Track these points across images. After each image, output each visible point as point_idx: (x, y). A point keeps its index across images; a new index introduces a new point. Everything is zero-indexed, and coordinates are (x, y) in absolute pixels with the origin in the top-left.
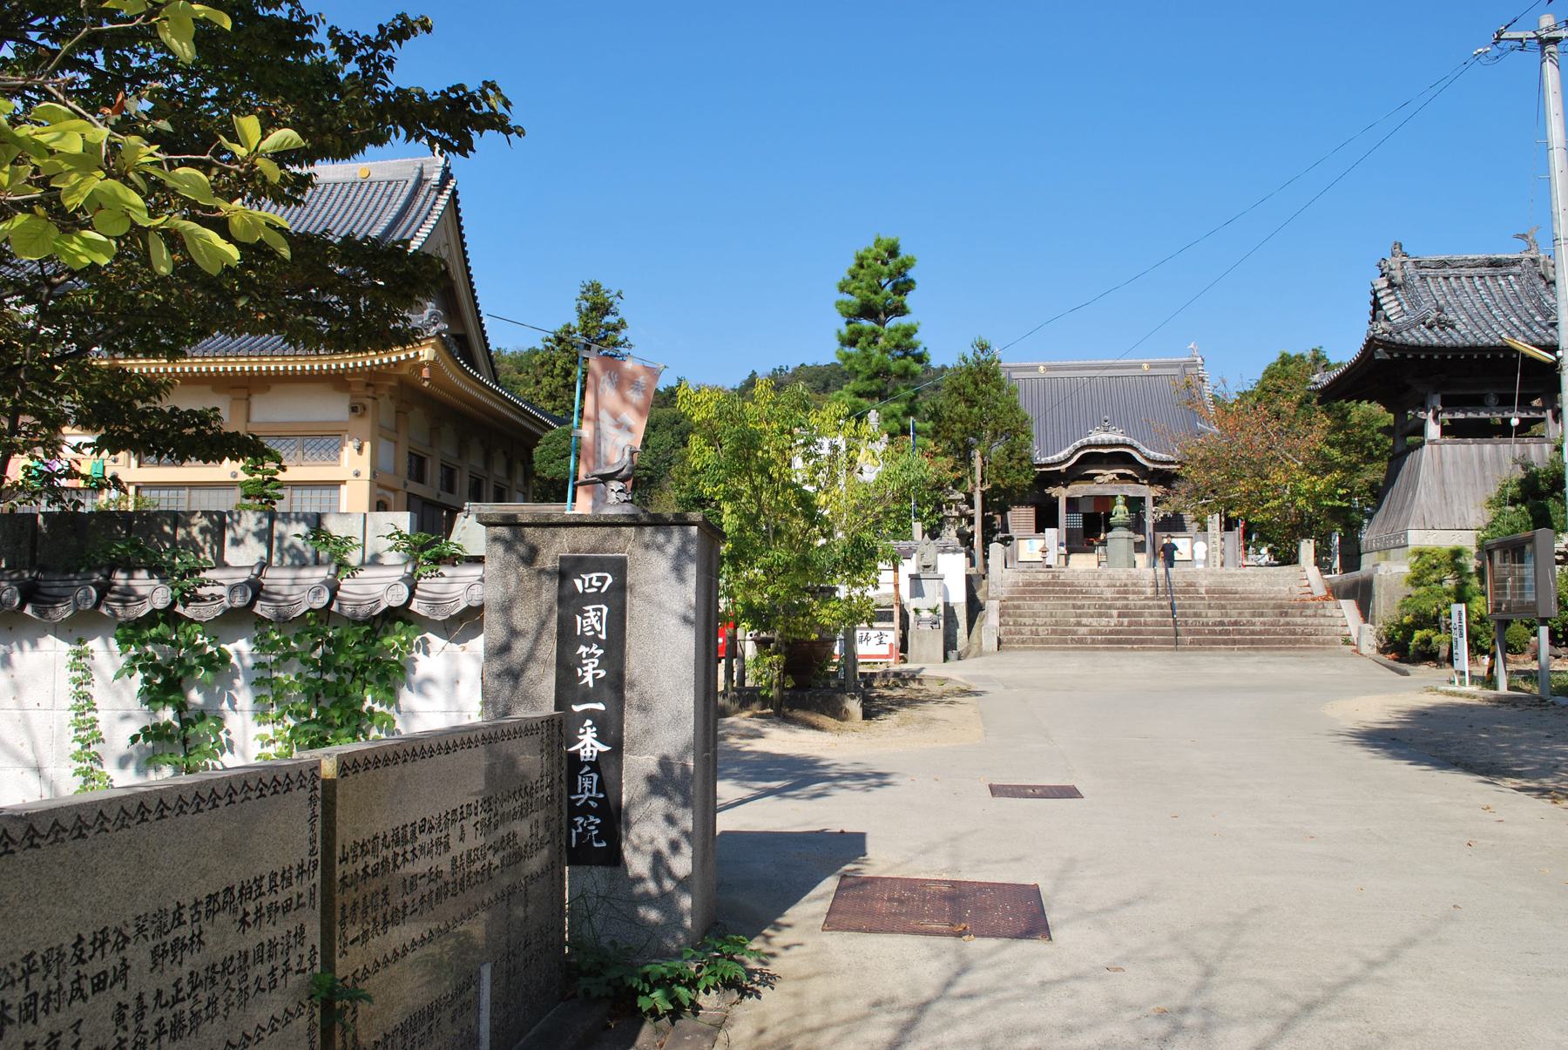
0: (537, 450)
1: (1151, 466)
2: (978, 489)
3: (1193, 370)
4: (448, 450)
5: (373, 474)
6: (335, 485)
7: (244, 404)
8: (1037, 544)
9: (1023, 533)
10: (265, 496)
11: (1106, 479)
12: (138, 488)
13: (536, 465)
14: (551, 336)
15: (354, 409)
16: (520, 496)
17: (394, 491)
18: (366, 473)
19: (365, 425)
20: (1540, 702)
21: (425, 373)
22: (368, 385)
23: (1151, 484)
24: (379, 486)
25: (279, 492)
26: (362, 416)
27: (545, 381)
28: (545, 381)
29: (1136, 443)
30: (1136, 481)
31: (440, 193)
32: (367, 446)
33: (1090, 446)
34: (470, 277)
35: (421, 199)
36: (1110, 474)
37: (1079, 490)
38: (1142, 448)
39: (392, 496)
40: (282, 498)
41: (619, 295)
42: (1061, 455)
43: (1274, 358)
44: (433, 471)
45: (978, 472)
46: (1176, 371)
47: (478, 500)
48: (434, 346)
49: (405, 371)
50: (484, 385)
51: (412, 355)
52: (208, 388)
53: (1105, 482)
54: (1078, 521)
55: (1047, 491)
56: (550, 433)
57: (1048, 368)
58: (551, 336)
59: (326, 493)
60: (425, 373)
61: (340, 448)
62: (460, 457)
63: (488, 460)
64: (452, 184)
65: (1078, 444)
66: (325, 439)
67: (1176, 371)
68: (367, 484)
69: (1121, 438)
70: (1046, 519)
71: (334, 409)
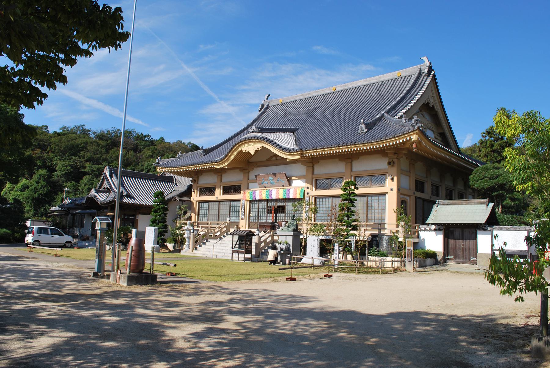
0: (471, 177)
4: (435, 178)
5: (398, 190)
6: (384, 194)
7: (350, 164)
10: (350, 199)
12: (315, 198)
13: (471, 183)
14: (485, 132)
15: (389, 164)
16: (471, 196)
17: (409, 196)
18: (395, 189)
19: (394, 170)
21: (414, 146)
22: (395, 153)
24: (401, 194)
25: (356, 198)
26: (393, 166)
27: (483, 150)
28: (483, 150)
31: (428, 76)
32: (395, 178)
34: (444, 109)
35: (422, 78)
39: (408, 198)
40: (356, 200)
41: (514, 112)
44: (428, 188)
47: (451, 198)
48: (417, 134)
49: (407, 146)
50: (453, 154)
51: (408, 139)
52: (337, 160)
56: (477, 169)
58: (485, 132)
59: (380, 198)
60: (414, 146)
61: (385, 180)
62: (441, 181)
63: (455, 182)
64: (433, 72)
66: (378, 177)
68: (396, 193)
71: (381, 164)
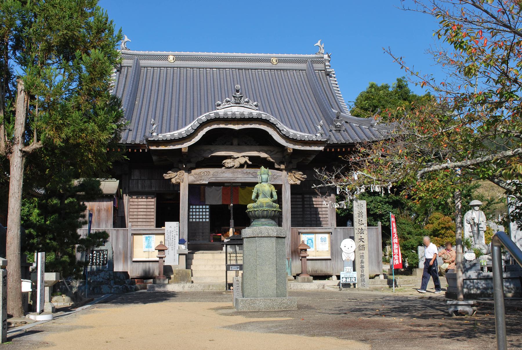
1: (291, 146)
2: (17, 148)
3: (321, 66)
8: (156, 240)
9: (140, 227)
11: (237, 163)
20: (426, 309)
23: (289, 170)
29: (273, 120)
30: (270, 165)
33: (217, 120)
36: (241, 157)
37: (204, 175)
38: (280, 125)
42: (181, 130)
43: (364, 88)
45: (20, 118)
46: (303, 66)
53: (235, 164)
54: (203, 215)
55: (167, 176)
57: (178, 58)
65: (203, 118)
67: (303, 66)
69: (255, 113)
70: (166, 212)
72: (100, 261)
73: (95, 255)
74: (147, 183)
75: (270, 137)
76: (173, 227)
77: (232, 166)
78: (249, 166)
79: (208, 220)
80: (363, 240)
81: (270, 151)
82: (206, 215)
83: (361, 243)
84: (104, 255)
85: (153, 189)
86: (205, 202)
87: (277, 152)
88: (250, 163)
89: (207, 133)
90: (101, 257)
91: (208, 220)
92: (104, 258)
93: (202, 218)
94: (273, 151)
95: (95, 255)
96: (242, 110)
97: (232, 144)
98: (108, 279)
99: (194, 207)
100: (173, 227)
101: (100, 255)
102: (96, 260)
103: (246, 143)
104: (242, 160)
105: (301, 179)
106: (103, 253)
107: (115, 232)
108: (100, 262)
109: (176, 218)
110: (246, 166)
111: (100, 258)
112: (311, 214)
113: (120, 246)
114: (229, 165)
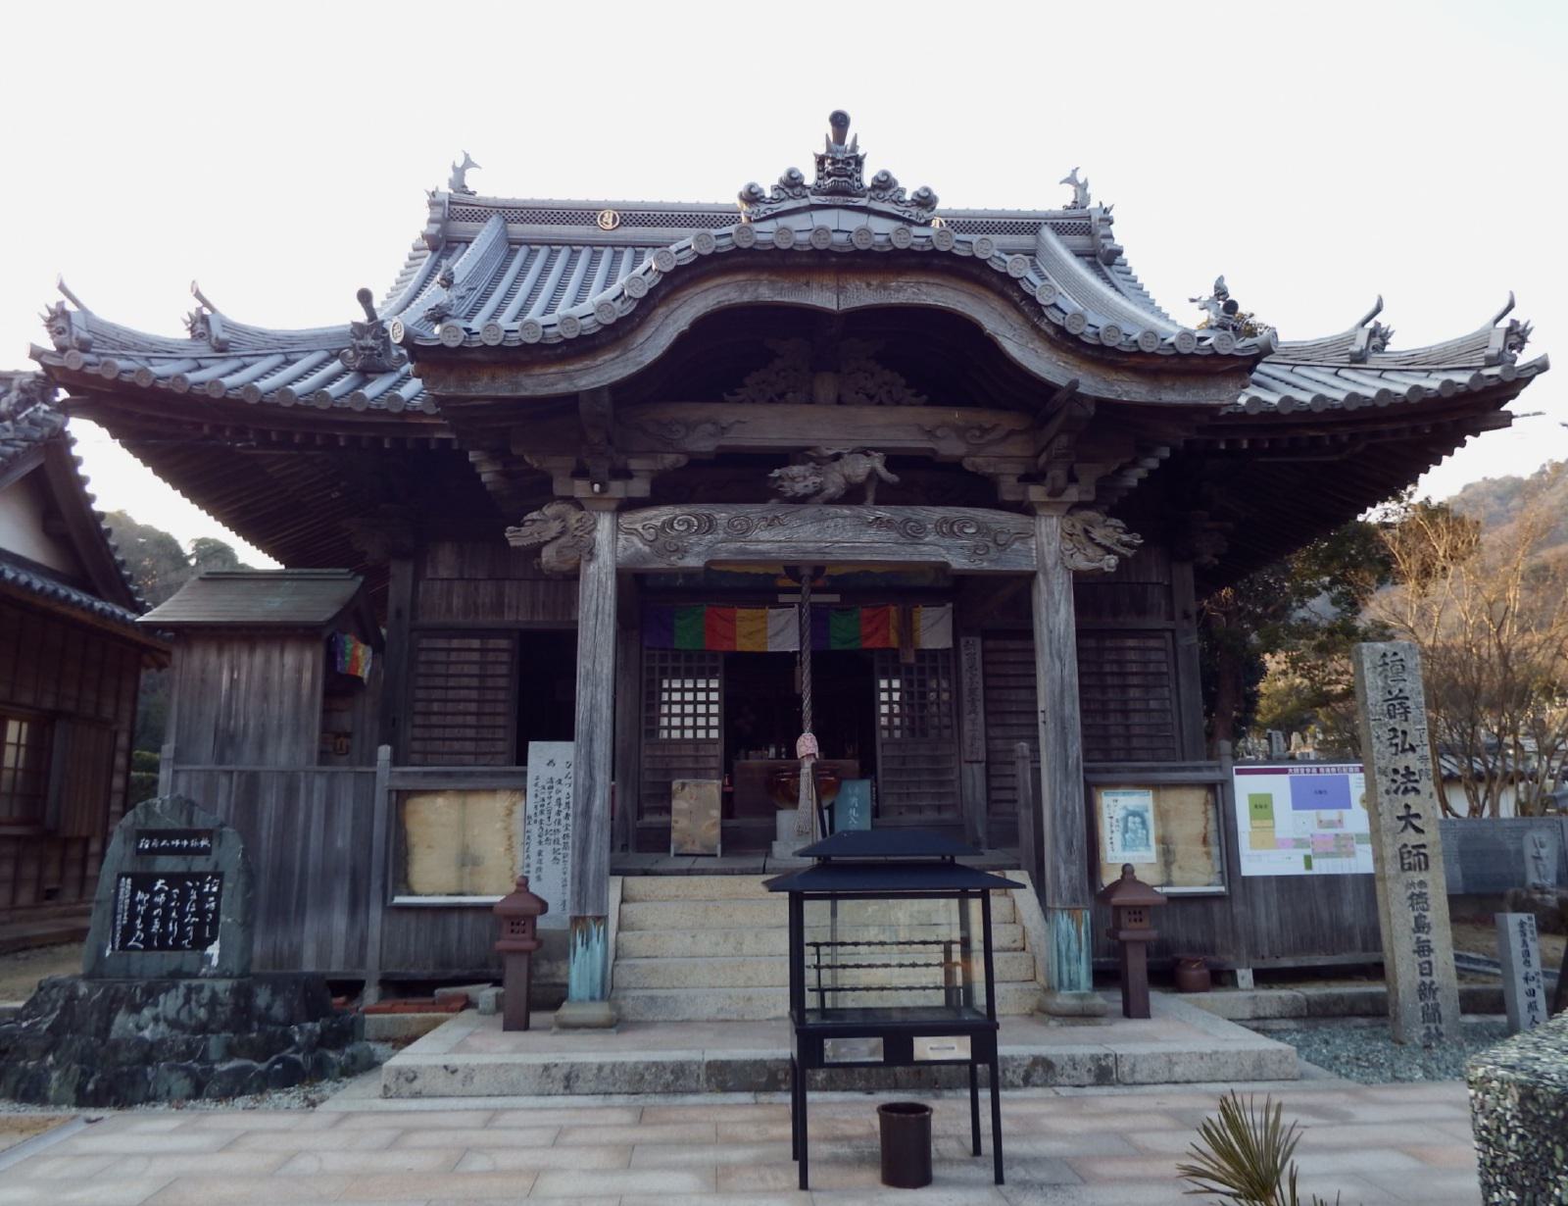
1: (1093, 384)
72: (182, 926)
73: (161, 899)
74: (486, 593)
75: (990, 345)
76: (560, 764)
77: (811, 489)
78: (887, 495)
79: (714, 734)
80: (1416, 822)
81: (980, 428)
82: (708, 715)
83: (1411, 838)
84: (202, 898)
85: (508, 618)
86: (358, 330)
87: (1011, 433)
88: (893, 478)
89: (703, 326)
90: (191, 908)
91: (714, 734)
92: (201, 912)
93: (695, 728)
94: (994, 428)
95: (161, 899)
96: (852, 221)
97: (811, 400)
98: (203, 1028)
99: (676, 684)
100: (560, 764)
101: (184, 898)
102: (165, 920)
103: (871, 398)
104: (860, 468)
105: (1124, 551)
106: (199, 890)
107: (320, 783)
108: (182, 934)
109: (561, 728)
110: (871, 496)
111: (182, 914)
112: (1125, 713)
113: (340, 843)
114: (800, 488)
